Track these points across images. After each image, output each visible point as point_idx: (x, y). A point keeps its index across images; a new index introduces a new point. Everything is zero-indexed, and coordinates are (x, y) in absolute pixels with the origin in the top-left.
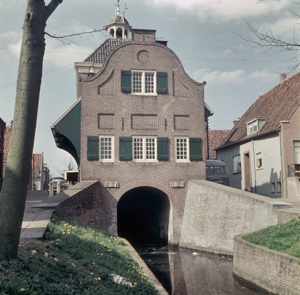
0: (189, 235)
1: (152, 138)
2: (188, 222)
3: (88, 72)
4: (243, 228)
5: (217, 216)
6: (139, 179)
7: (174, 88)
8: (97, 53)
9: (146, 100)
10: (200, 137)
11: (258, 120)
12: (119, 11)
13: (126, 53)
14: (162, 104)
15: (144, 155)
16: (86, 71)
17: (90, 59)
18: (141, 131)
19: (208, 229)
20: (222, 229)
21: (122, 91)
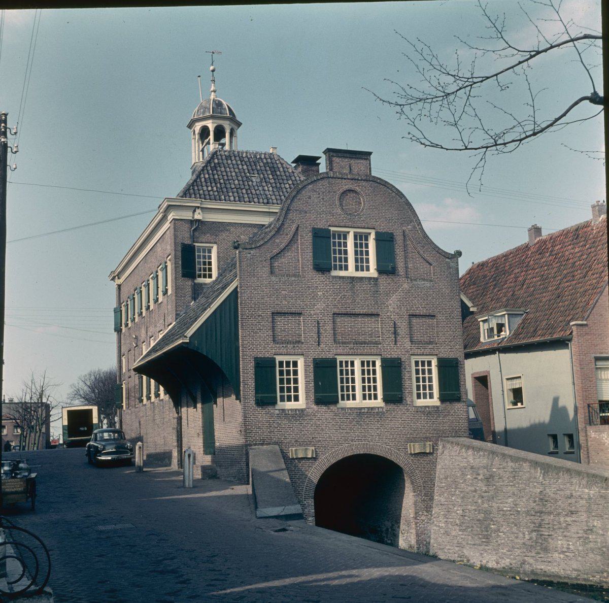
0: (452, 546)
1: (371, 358)
2: (445, 520)
3: (191, 218)
4: (585, 532)
5: (519, 509)
6: (352, 440)
7: (406, 263)
8: (200, 179)
9: (358, 286)
10: (456, 357)
11: (508, 314)
12: (214, 91)
13: (319, 194)
14: (388, 294)
15: (359, 392)
16: (187, 215)
17: (192, 191)
18: (352, 346)
19: (500, 534)
20: (534, 534)
21: (314, 268)
